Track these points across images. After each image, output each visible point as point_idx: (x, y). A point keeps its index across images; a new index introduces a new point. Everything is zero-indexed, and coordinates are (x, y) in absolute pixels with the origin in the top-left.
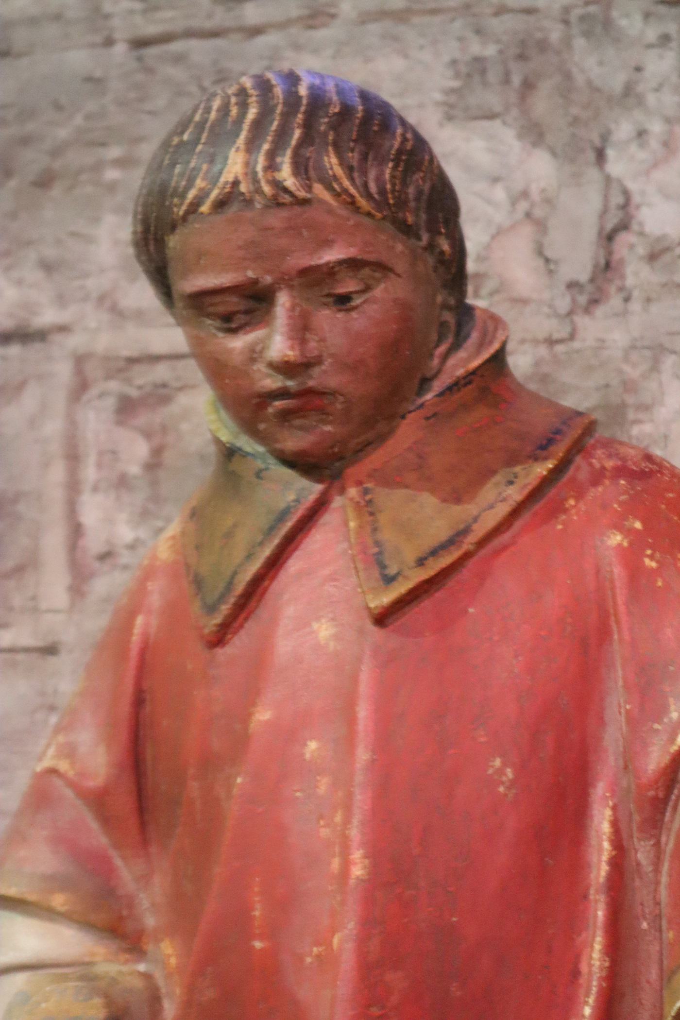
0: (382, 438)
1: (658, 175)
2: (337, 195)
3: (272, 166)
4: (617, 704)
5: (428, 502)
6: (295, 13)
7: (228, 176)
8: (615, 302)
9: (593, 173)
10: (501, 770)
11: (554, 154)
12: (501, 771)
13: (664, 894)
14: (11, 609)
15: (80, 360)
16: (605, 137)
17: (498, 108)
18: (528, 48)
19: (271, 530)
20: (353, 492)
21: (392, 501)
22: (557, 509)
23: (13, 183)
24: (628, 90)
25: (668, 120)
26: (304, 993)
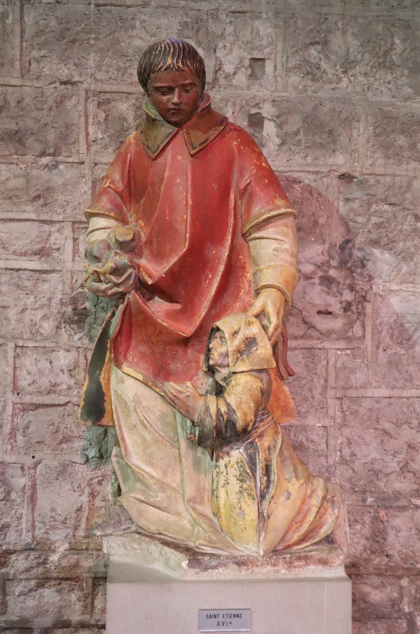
0: (190, 119)
1: (228, 57)
2: (189, 70)
3: (177, 62)
4: (235, 174)
5: (200, 133)
6: (140, 3)
7: (168, 63)
8: (217, 88)
9: (213, 55)
10: (215, 186)
11: (204, 49)
12: (215, 186)
13: (243, 210)
14: (72, 153)
15: (87, 91)
16: (216, 46)
17: (191, 36)
18: (199, 20)
19: (166, 138)
20: (184, 130)
21: (193, 133)
22: (224, 136)
23: (65, 41)
24: (222, 35)
25: (231, 44)
26: (177, 227)
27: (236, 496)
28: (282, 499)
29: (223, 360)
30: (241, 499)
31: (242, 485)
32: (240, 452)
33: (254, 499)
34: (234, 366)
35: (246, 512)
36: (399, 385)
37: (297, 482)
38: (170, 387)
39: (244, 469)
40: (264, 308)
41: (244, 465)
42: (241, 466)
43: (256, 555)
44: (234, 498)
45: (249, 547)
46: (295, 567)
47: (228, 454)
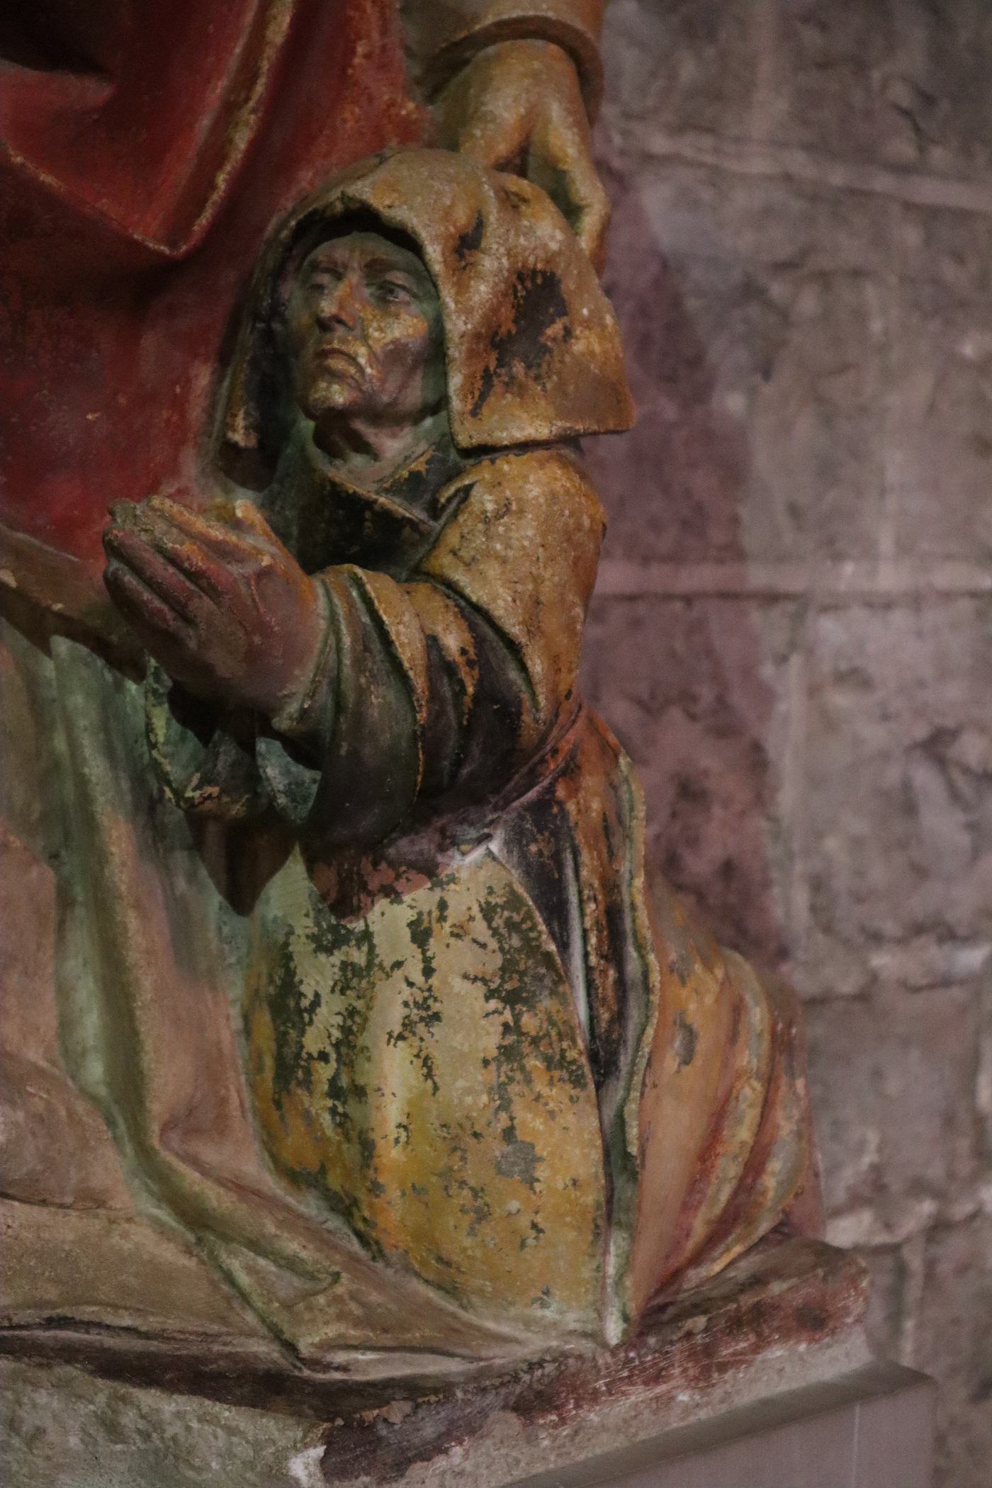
27: (481, 1076)
28: (670, 1062)
29: (403, 387)
30: (514, 1089)
31: (517, 1018)
32: (490, 853)
33: (578, 1081)
34: (475, 413)
35: (541, 1150)
36: (664, 544)
37: (708, 978)
38: (160, 527)
39: (527, 941)
40: (528, 136)
41: (529, 916)
42: (510, 925)
43: (586, 1346)
44: (468, 1090)
45: (549, 1314)
46: (723, 1368)
47: (429, 870)
